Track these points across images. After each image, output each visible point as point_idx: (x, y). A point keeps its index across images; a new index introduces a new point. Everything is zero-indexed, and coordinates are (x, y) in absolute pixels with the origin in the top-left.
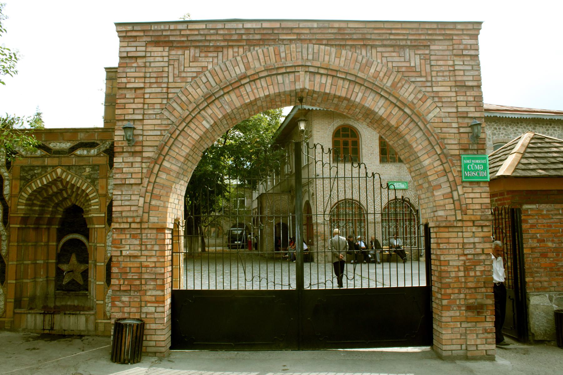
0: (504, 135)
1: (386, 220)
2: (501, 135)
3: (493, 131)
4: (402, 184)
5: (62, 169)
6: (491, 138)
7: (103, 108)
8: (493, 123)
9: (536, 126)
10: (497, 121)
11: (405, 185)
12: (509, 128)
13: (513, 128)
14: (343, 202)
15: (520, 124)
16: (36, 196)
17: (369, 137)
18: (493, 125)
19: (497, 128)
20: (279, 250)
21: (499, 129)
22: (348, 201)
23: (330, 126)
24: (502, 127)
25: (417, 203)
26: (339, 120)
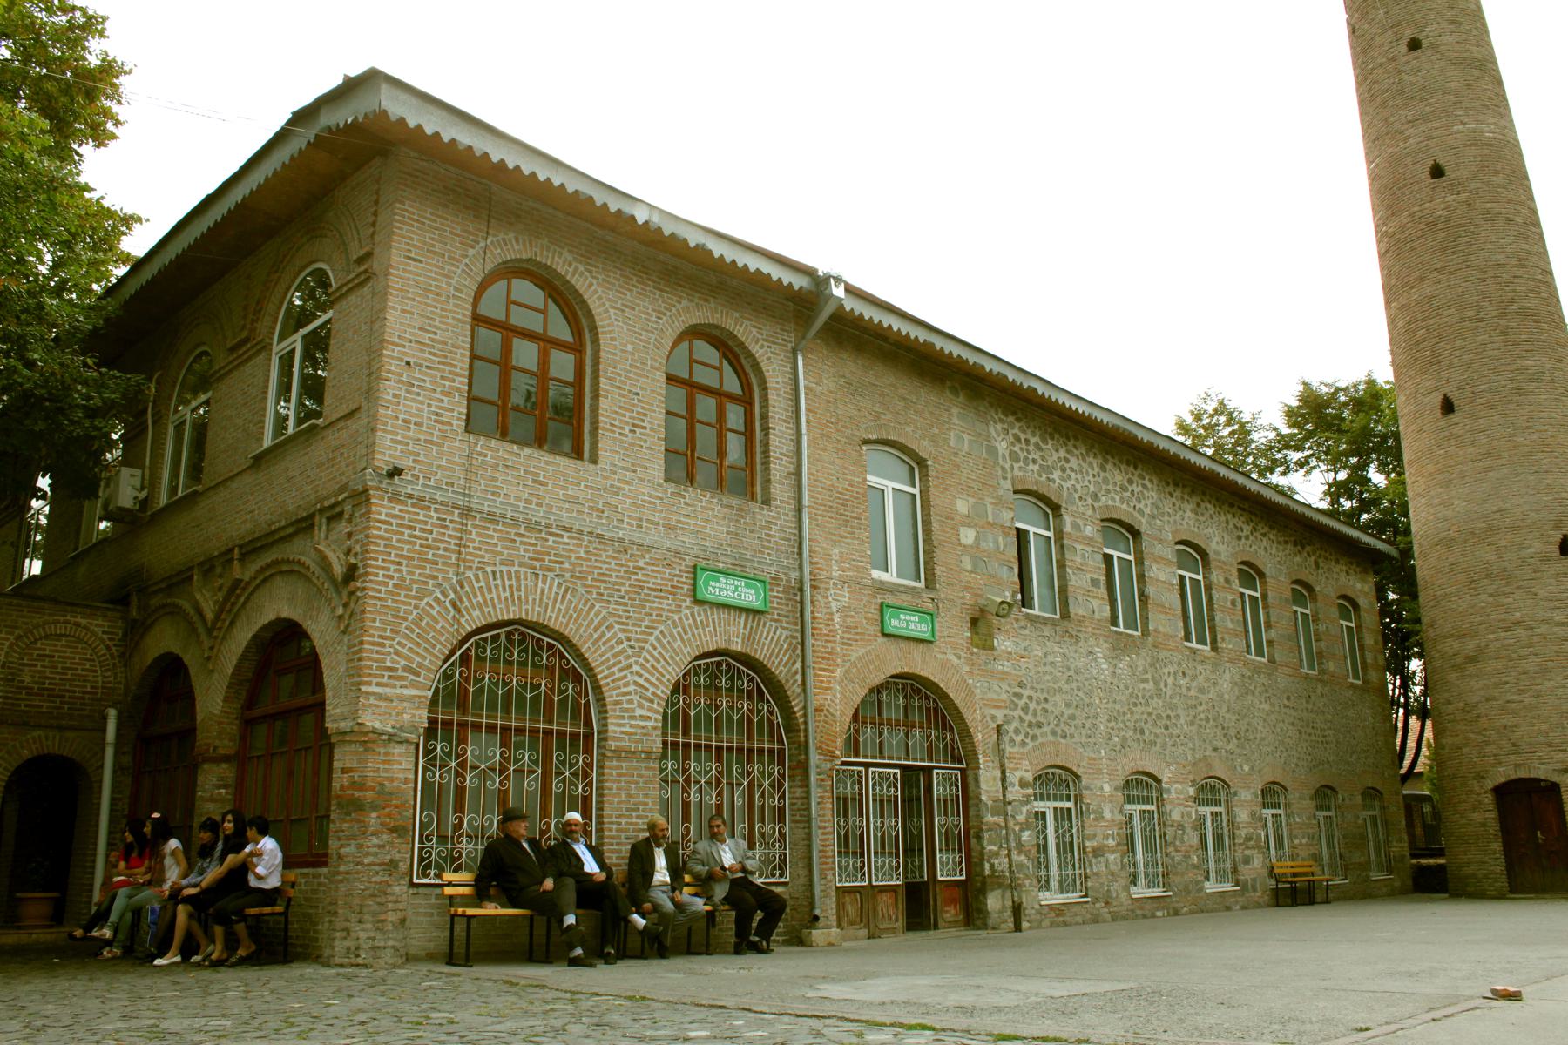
0: (1037, 467)
1: (761, 751)
2: (1031, 467)
3: (1012, 444)
4: (747, 585)
5: (64, 154)
6: (1007, 466)
7: (1521, 137)
8: (1011, 418)
9: (1106, 461)
10: (1020, 415)
11: (757, 593)
12: (1050, 446)
13: (1057, 451)
14: (495, 638)
15: (1072, 442)
16: (1236, 454)
17: (630, 348)
18: (1012, 426)
19: (1022, 436)
20: (427, 876)
21: (1027, 441)
22: (522, 634)
23: (471, 252)
24: (1033, 440)
25: (799, 677)
26: (511, 235)
